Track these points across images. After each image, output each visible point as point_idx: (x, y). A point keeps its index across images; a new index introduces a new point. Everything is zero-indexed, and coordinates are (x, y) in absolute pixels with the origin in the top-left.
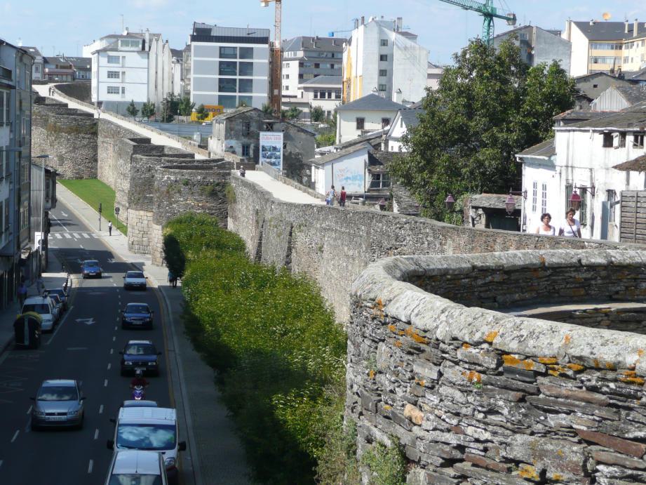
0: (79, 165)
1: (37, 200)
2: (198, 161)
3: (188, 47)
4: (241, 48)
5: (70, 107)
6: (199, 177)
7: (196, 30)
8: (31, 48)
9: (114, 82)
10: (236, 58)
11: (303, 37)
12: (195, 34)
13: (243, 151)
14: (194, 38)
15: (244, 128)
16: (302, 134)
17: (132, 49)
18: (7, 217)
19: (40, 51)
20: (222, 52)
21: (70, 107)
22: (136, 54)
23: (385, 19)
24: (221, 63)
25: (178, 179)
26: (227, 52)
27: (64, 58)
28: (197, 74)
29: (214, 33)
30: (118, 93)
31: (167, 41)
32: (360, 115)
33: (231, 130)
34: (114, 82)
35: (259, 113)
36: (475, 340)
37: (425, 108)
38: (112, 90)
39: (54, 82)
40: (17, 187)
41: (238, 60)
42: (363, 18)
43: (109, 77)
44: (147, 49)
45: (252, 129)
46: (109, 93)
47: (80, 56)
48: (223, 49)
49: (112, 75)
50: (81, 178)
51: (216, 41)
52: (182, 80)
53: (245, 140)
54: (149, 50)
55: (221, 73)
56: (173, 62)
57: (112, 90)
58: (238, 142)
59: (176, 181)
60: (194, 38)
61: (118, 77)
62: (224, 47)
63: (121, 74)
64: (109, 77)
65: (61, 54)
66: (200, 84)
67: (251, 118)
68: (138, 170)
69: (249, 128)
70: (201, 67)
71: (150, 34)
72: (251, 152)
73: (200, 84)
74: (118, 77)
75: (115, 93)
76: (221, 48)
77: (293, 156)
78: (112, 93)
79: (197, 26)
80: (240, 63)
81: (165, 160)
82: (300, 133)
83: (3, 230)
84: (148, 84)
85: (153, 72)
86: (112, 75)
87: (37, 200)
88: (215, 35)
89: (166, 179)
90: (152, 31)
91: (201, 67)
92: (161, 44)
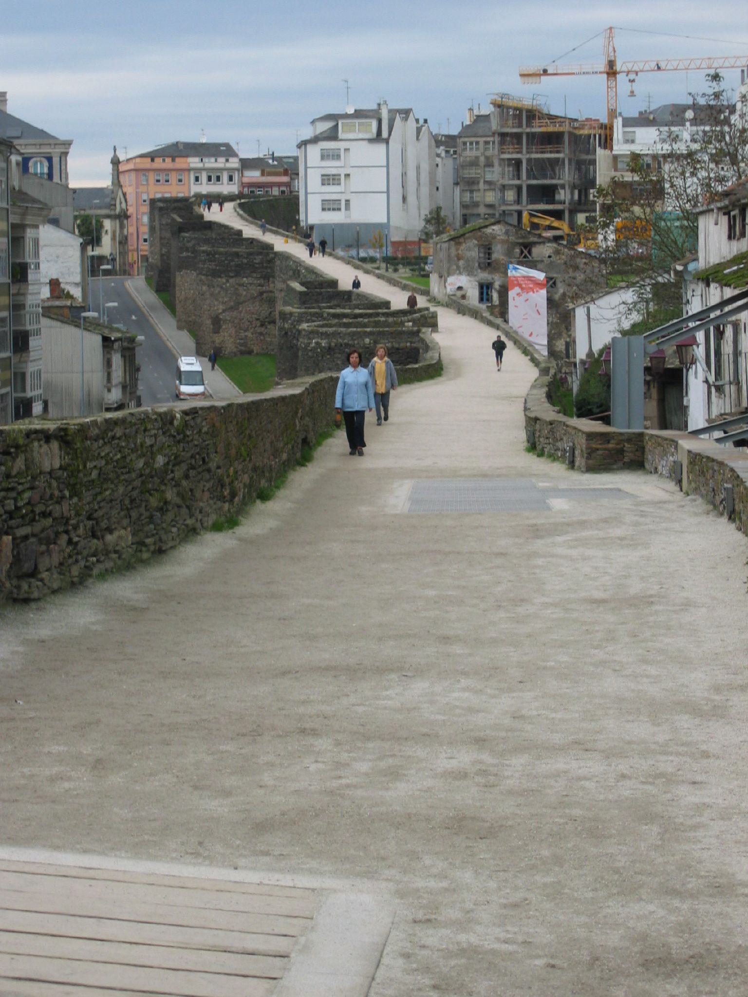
0: (245, 331)
1: (89, 391)
6: (367, 341)
9: (332, 192)
11: (673, 105)
13: (481, 294)
15: (482, 255)
17: (361, 136)
19: (235, 147)
22: (365, 143)
25: (333, 344)
27: (274, 159)
28: (535, 178)
30: (339, 209)
31: (426, 121)
33: (459, 259)
34: (332, 192)
35: (509, 228)
36: (527, 755)
38: (329, 206)
43: (323, 184)
44: (385, 134)
45: (494, 256)
46: (323, 209)
49: (329, 179)
50: (250, 352)
53: (485, 276)
54: (390, 134)
56: (438, 155)
57: (329, 206)
58: (472, 279)
59: (330, 348)
61: (339, 184)
63: (343, 177)
64: (323, 184)
67: (494, 238)
68: (286, 333)
69: (489, 254)
71: (390, 111)
72: (495, 296)
74: (339, 184)
75: (334, 209)
81: (329, 314)
85: (396, 172)
86: (329, 179)
87: (89, 391)
89: (313, 345)
92: (411, 125)
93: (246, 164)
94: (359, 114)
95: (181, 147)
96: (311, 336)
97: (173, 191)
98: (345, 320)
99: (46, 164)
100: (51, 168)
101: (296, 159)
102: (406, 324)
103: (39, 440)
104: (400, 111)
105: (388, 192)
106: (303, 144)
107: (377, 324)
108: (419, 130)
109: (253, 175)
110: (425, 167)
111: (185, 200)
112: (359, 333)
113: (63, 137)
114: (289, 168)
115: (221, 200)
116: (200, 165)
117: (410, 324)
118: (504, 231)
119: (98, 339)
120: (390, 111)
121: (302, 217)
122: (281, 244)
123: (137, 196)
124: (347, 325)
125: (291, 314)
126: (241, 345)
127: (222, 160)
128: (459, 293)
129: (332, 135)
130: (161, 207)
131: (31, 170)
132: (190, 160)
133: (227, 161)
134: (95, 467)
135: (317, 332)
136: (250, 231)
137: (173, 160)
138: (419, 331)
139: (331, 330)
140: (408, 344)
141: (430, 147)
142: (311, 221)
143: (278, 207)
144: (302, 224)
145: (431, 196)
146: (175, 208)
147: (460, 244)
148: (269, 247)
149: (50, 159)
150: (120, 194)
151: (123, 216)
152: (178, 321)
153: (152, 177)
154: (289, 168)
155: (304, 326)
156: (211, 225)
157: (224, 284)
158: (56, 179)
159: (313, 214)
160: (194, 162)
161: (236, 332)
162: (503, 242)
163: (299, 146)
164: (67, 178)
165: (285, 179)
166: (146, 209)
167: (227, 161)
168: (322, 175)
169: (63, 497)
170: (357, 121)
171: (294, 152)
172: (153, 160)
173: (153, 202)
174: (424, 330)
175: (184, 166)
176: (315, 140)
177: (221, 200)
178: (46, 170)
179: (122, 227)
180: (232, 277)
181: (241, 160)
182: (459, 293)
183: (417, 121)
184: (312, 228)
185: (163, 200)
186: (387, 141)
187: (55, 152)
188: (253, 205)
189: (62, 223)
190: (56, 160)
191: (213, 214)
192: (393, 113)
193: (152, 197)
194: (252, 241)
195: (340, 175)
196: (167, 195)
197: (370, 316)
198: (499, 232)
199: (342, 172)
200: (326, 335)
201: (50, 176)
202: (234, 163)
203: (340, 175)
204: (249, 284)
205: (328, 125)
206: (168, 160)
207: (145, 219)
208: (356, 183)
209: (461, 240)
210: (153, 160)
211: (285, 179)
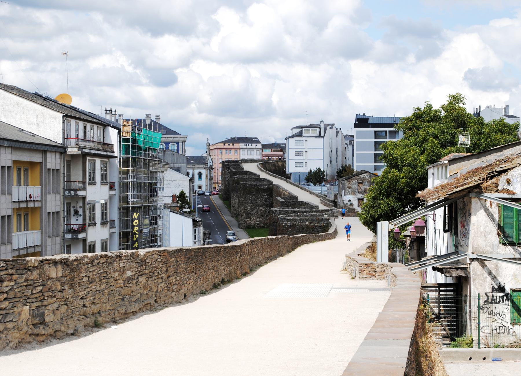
7: (358, 119)
8: (254, 138)
12: (357, 122)
14: (356, 126)
21: (261, 177)
23: (496, 107)
24: (376, 143)
29: (370, 122)
31: (340, 129)
33: (349, 188)
37: (428, 169)
41: (130, 156)
42: (480, 106)
44: (322, 135)
49: (299, 153)
51: (372, 127)
53: (360, 196)
55: (376, 149)
56: (346, 144)
57: (299, 164)
60: (356, 126)
66: (362, 158)
67: (365, 179)
70: (362, 147)
71: (324, 125)
73: (362, 158)
76: (375, 132)
79: (359, 117)
84: (323, 159)
85: (327, 150)
86: (299, 153)
90: (326, 122)
91: (362, 147)
92: (334, 131)
93: (265, 146)
94: (311, 126)
95: (236, 139)
97: (233, 157)
98: (298, 214)
99: (176, 145)
100: (178, 147)
101: (285, 144)
103: (49, 264)
104: (329, 125)
105: (323, 159)
106: (287, 138)
107: (312, 216)
108: (337, 133)
109: (268, 152)
110: (340, 149)
111: (237, 162)
112: (303, 219)
113: (183, 134)
114: (282, 148)
115: (252, 161)
116: (245, 147)
119: (191, 220)
120: (324, 125)
121: (287, 170)
122: (276, 181)
123: (217, 160)
124: (299, 216)
125: (276, 211)
126: (258, 224)
127: (254, 145)
128: (350, 203)
129: (300, 135)
130: (226, 165)
131: (170, 148)
132: (241, 144)
134: (86, 276)
135: (286, 219)
136: (263, 175)
137: (233, 145)
138: (329, 219)
139: (291, 218)
141: (342, 140)
142: (290, 171)
143: (280, 171)
144: (287, 172)
145: (342, 161)
147: (350, 181)
148: (271, 182)
149: (178, 144)
150: (210, 159)
151: (211, 168)
153: (224, 151)
154: (282, 148)
155: (280, 216)
156: (247, 173)
158: (180, 152)
159: (291, 168)
160: (242, 145)
163: (286, 139)
164: (185, 152)
165: (281, 153)
166: (221, 165)
170: (310, 129)
171: (284, 142)
172: (224, 145)
173: (223, 162)
174: (331, 218)
175: (238, 147)
176: (293, 137)
177: (252, 161)
178: (176, 148)
179: (210, 173)
181: (262, 145)
182: (350, 203)
183: (337, 129)
184: (291, 174)
185: (228, 162)
186: (323, 137)
187: (180, 140)
188: (266, 165)
189: (182, 170)
190: (180, 144)
191: (247, 167)
192: (326, 126)
193: (223, 160)
194: (264, 180)
196: (230, 160)
197: (309, 212)
198: (367, 177)
199: (304, 150)
200: (288, 220)
201: (178, 151)
202: (259, 146)
204: (261, 199)
205: (299, 130)
206: (231, 144)
207: (220, 170)
208: (310, 155)
209: (350, 180)
210: (224, 145)
211: (281, 153)
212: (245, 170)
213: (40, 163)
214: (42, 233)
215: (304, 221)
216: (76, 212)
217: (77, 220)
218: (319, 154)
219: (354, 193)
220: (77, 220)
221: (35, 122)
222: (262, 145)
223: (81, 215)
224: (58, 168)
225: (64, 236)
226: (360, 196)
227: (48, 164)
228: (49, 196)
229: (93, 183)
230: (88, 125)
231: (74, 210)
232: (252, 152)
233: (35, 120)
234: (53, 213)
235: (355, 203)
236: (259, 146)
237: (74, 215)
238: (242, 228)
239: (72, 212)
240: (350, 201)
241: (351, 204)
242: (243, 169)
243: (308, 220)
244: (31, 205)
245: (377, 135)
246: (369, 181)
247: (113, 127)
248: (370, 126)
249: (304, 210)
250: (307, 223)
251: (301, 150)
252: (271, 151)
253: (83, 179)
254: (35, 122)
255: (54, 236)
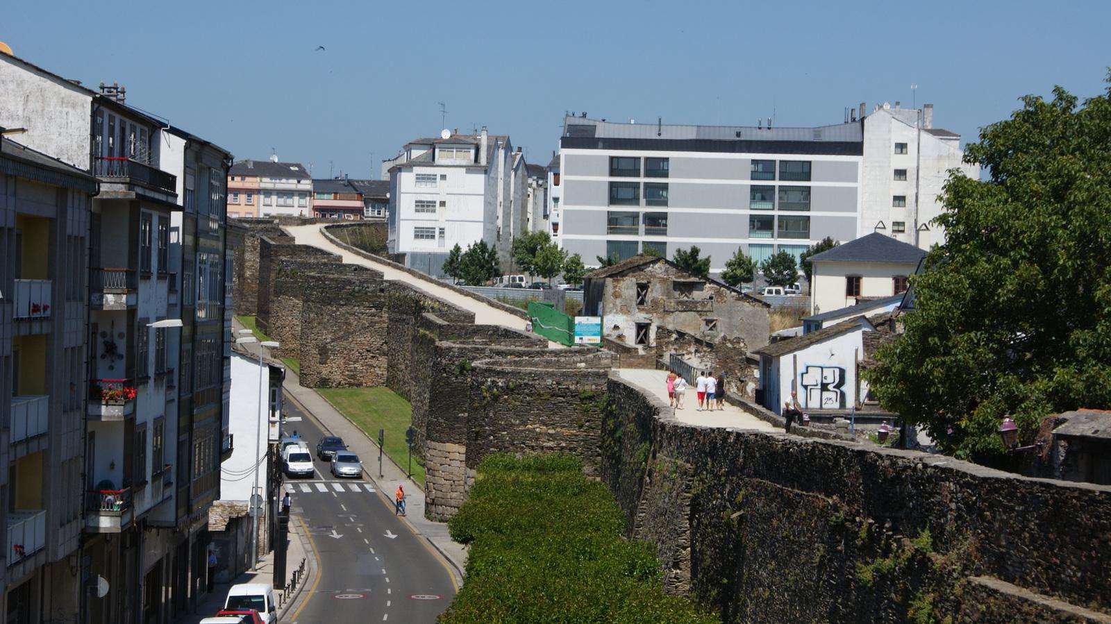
0: (355, 363)
2: (551, 352)
3: (557, 159)
4: (647, 159)
5: (479, 321)
8: (293, 165)
9: (425, 219)
10: (638, 175)
14: (567, 143)
16: (746, 304)
18: (158, 453)
20: (615, 166)
21: (345, 261)
26: (623, 166)
30: (433, 237)
32: (854, 271)
34: (425, 219)
39: (327, 222)
40: (186, 396)
41: (777, 183)
44: (483, 161)
47: (376, 179)
48: (615, 160)
51: (605, 147)
52: (887, 455)
62: (618, 158)
65: (343, 176)
66: (576, 222)
67: (654, 277)
70: (575, 193)
73: (576, 222)
76: (612, 159)
77: (729, 345)
78: (422, 237)
80: (646, 184)
81: (491, 350)
82: (740, 303)
83: (149, 477)
88: (602, 136)
93: (322, 186)
95: (250, 166)
96: (487, 374)
102: (578, 365)
117: (583, 365)
118: (663, 269)
125: (450, 349)
128: (617, 333)
132: (264, 180)
133: (299, 182)
136: (349, 258)
140: (594, 387)
143: (375, 241)
146: (262, 230)
147: (618, 281)
152: (1082, 407)
157: (335, 312)
159: (406, 242)
161: (345, 363)
162: (663, 281)
167: (299, 182)
168: (416, 202)
169: (452, 608)
180: (343, 305)
182: (617, 333)
184: (404, 255)
195: (435, 202)
199: (438, 199)
203: (435, 202)
212: (297, 242)
213: (51, 219)
214: (50, 402)
215: (541, 376)
216: (111, 348)
217: (111, 368)
218: (477, 208)
219: (625, 310)
220: (111, 368)
221: (20, 113)
222: (314, 181)
223: (121, 357)
224: (82, 234)
225: (86, 409)
226: (642, 317)
227: (69, 223)
228: (67, 305)
229: (147, 276)
230: (128, 122)
231: (106, 343)
232: (289, 201)
233: (21, 108)
234: (73, 349)
235: (630, 339)
236: (306, 185)
237: (103, 357)
238: (308, 386)
239: (100, 350)
240: (616, 327)
241: (620, 337)
242: (293, 239)
243: (552, 375)
244: (36, 329)
245: (615, 167)
246: (663, 281)
247: (174, 131)
248: (600, 144)
249: (523, 349)
250: (549, 382)
251: (429, 198)
252: (335, 199)
253: (130, 266)
254: (20, 113)
255: (72, 409)
